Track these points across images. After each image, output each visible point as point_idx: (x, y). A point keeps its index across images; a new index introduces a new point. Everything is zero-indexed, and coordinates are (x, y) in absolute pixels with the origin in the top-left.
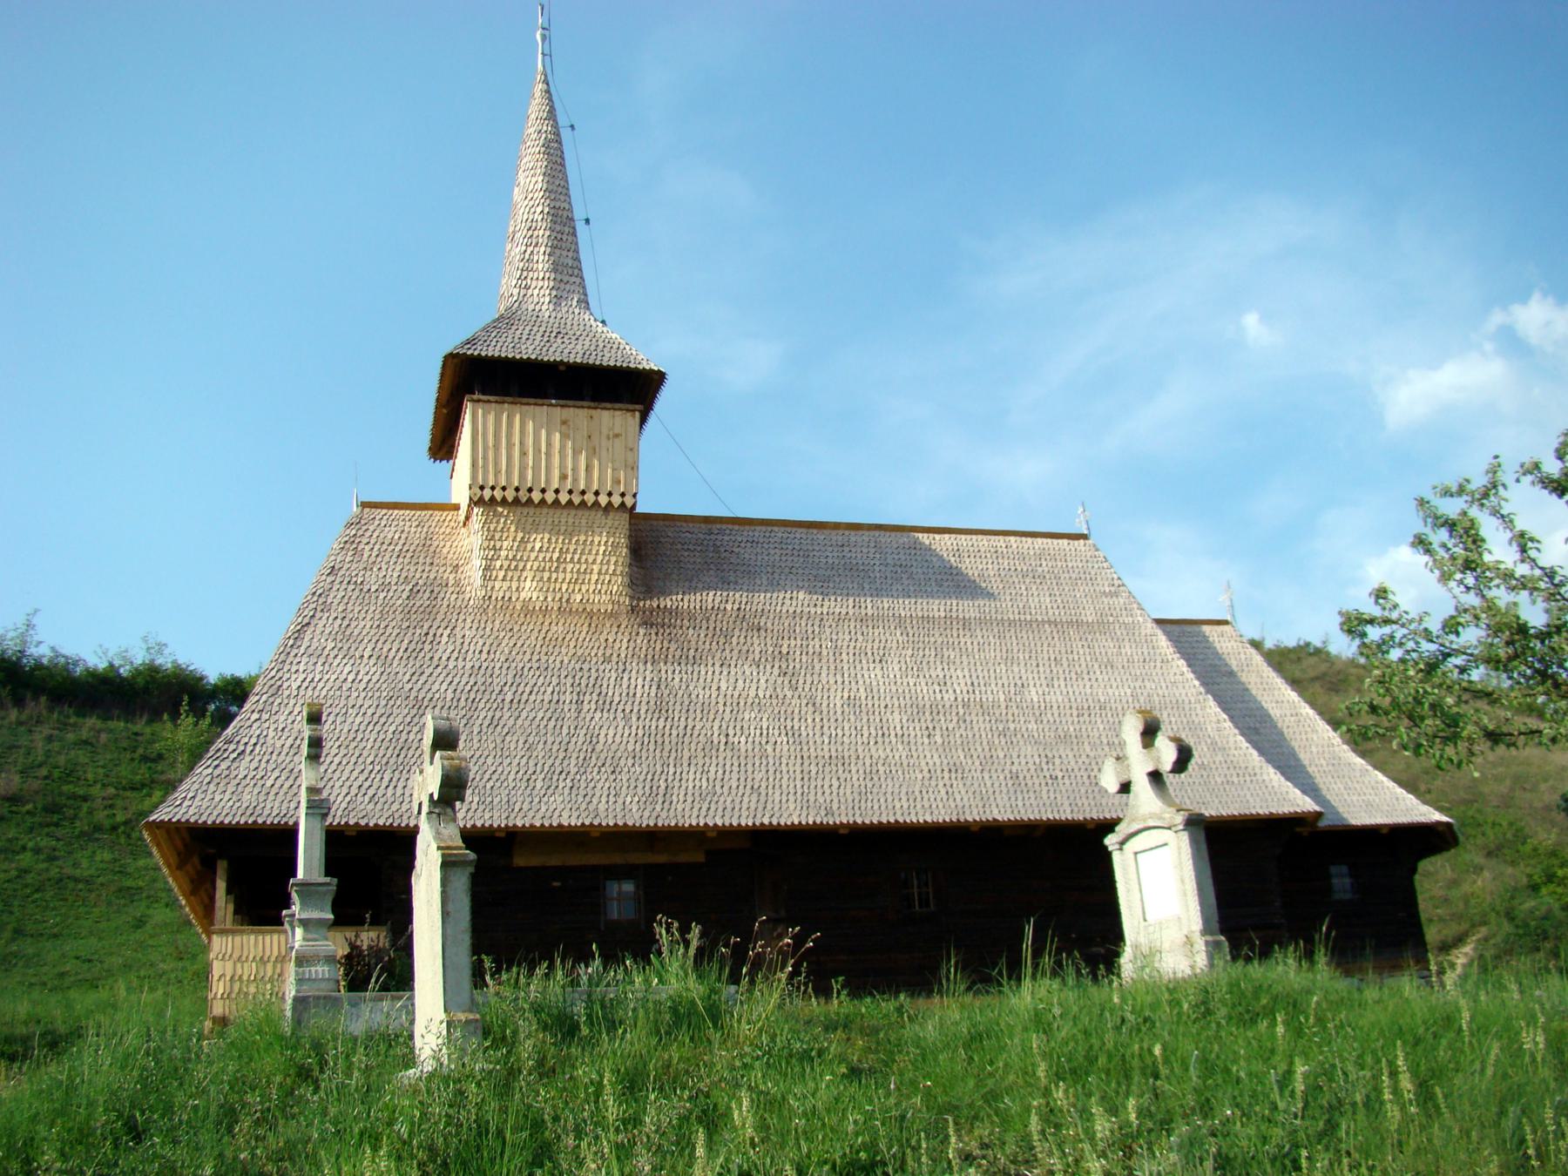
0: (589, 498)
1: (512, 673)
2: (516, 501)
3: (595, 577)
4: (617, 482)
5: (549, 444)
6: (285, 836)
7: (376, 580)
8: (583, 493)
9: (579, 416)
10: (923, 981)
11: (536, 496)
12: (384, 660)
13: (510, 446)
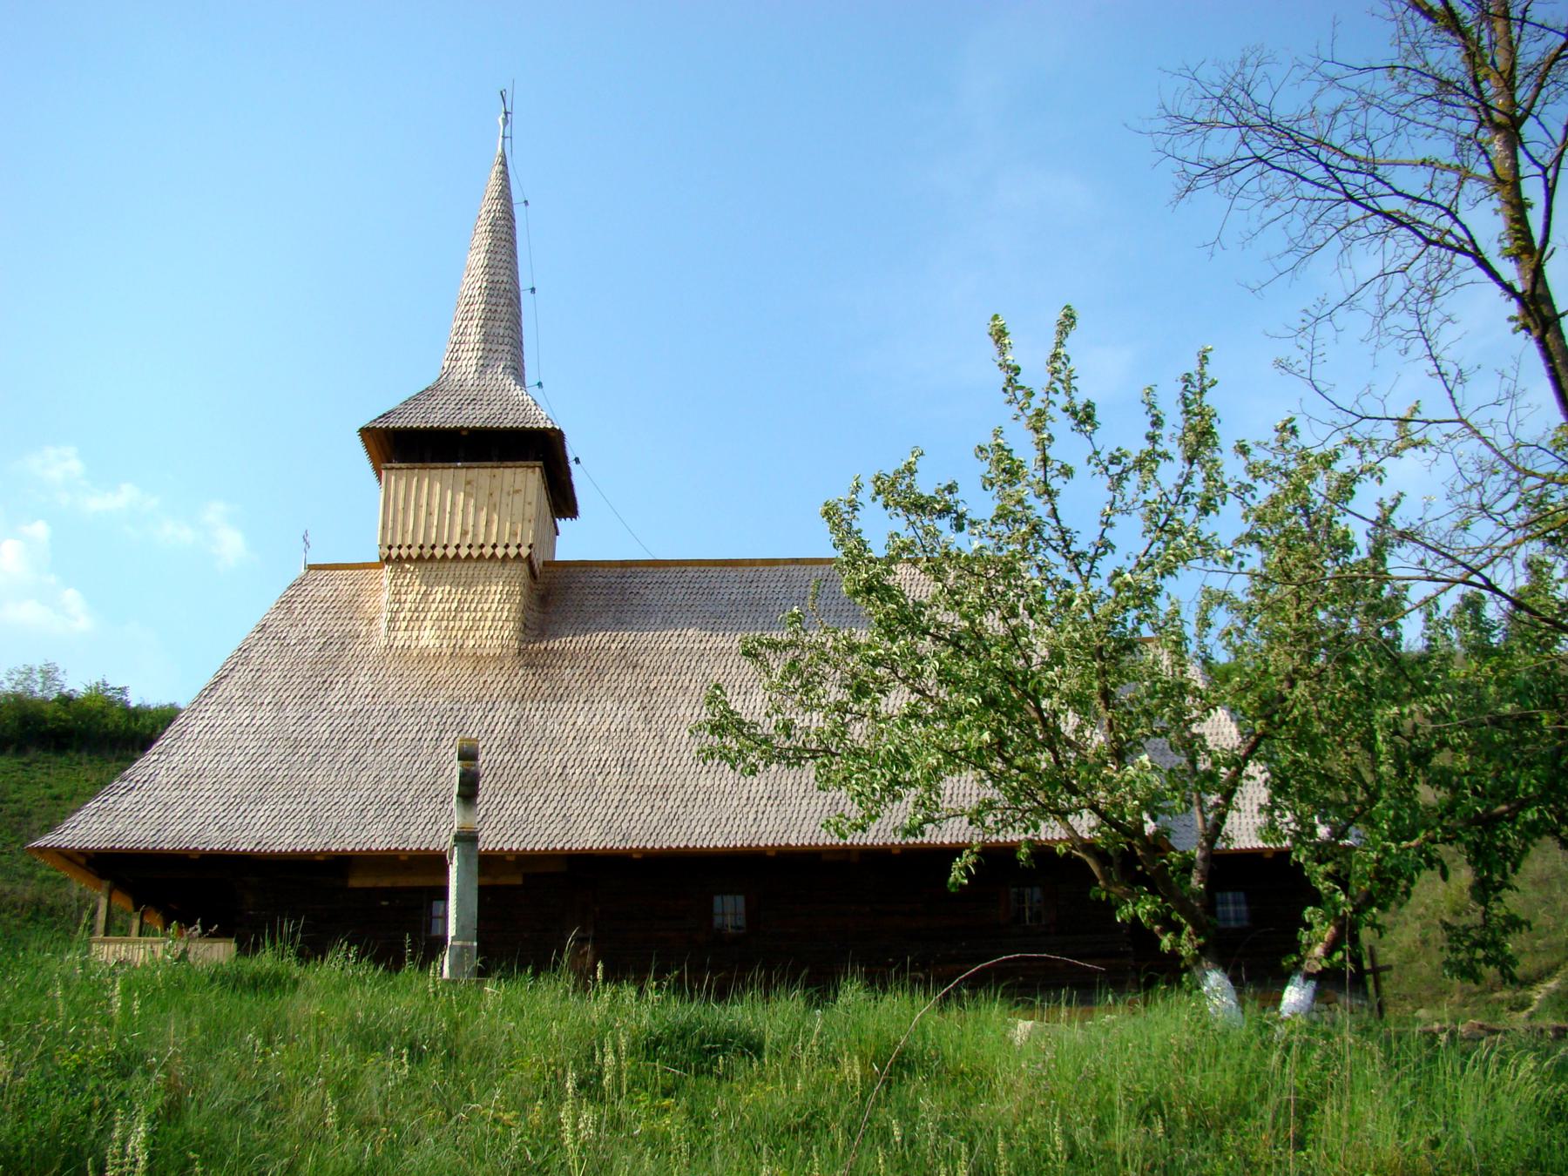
0: (488, 551)
1: (388, 713)
2: (420, 558)
3: (488, 623)
4: (513, 534)
5: (453, 504)
6: (438, 862)
7: (305, 638)
8: (482, 546)
9: (482, 475)
10: (822, 986)
11: (439, 552)
12: (280, 706)
13: (418, 506)
